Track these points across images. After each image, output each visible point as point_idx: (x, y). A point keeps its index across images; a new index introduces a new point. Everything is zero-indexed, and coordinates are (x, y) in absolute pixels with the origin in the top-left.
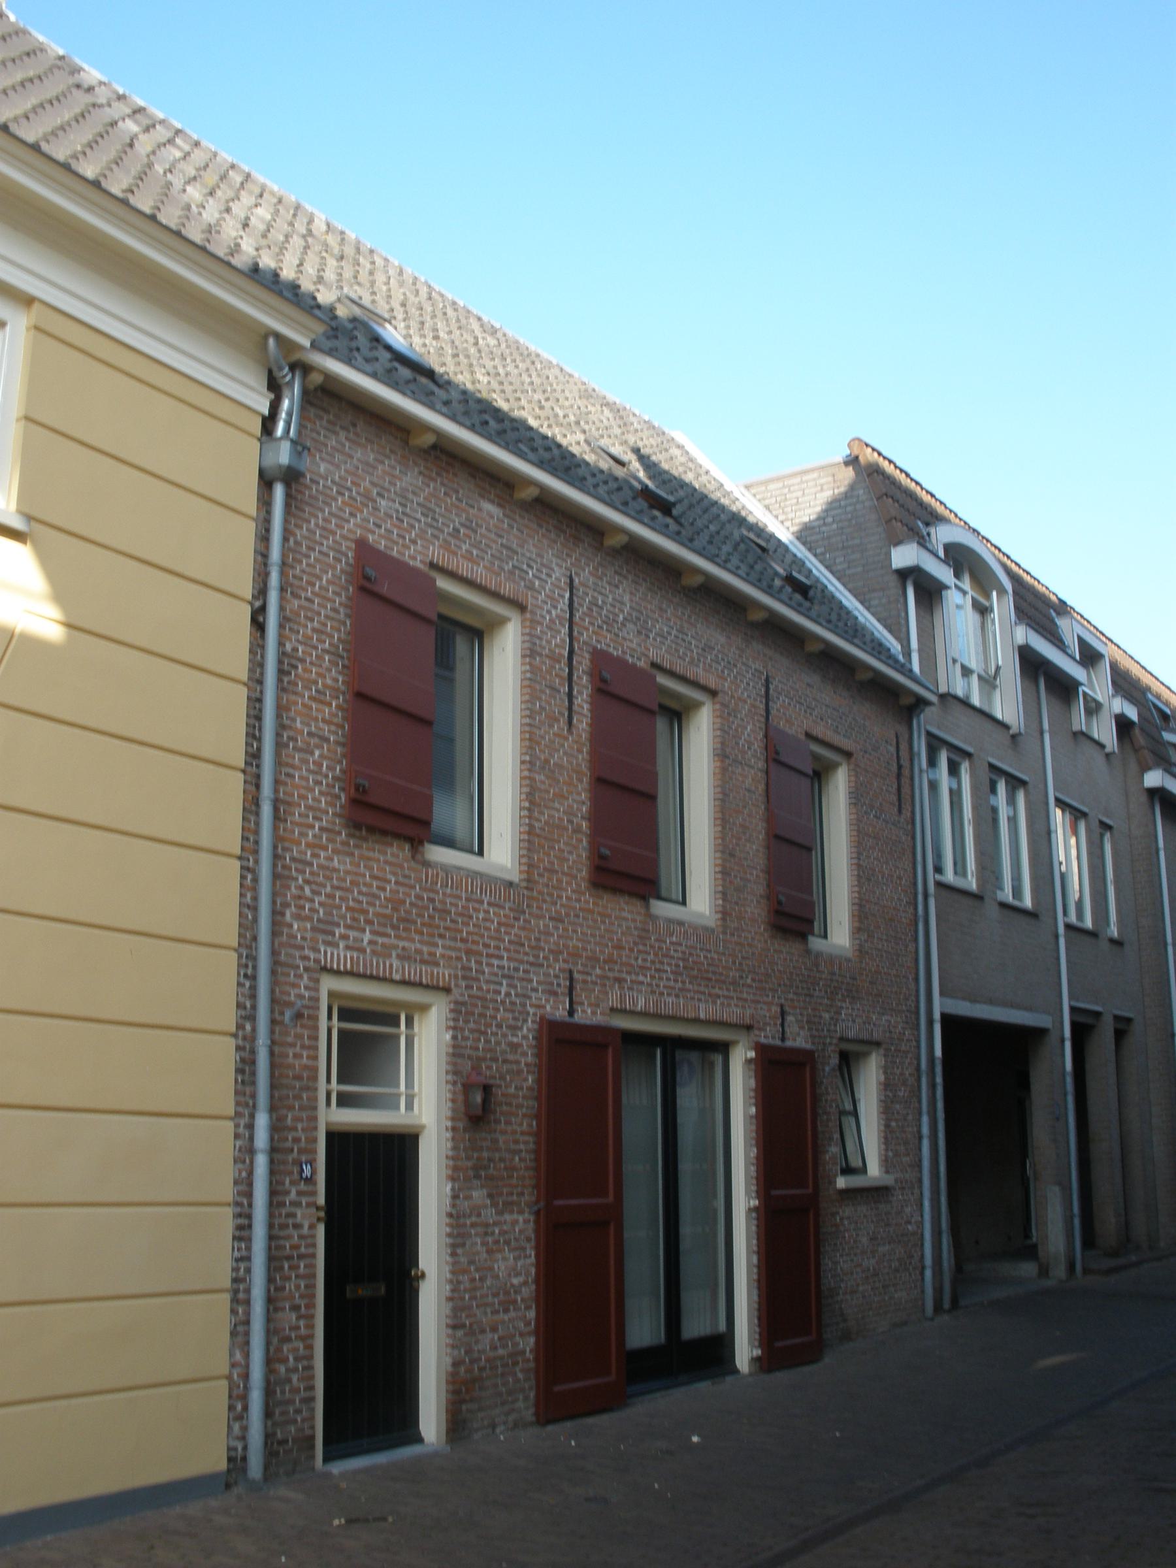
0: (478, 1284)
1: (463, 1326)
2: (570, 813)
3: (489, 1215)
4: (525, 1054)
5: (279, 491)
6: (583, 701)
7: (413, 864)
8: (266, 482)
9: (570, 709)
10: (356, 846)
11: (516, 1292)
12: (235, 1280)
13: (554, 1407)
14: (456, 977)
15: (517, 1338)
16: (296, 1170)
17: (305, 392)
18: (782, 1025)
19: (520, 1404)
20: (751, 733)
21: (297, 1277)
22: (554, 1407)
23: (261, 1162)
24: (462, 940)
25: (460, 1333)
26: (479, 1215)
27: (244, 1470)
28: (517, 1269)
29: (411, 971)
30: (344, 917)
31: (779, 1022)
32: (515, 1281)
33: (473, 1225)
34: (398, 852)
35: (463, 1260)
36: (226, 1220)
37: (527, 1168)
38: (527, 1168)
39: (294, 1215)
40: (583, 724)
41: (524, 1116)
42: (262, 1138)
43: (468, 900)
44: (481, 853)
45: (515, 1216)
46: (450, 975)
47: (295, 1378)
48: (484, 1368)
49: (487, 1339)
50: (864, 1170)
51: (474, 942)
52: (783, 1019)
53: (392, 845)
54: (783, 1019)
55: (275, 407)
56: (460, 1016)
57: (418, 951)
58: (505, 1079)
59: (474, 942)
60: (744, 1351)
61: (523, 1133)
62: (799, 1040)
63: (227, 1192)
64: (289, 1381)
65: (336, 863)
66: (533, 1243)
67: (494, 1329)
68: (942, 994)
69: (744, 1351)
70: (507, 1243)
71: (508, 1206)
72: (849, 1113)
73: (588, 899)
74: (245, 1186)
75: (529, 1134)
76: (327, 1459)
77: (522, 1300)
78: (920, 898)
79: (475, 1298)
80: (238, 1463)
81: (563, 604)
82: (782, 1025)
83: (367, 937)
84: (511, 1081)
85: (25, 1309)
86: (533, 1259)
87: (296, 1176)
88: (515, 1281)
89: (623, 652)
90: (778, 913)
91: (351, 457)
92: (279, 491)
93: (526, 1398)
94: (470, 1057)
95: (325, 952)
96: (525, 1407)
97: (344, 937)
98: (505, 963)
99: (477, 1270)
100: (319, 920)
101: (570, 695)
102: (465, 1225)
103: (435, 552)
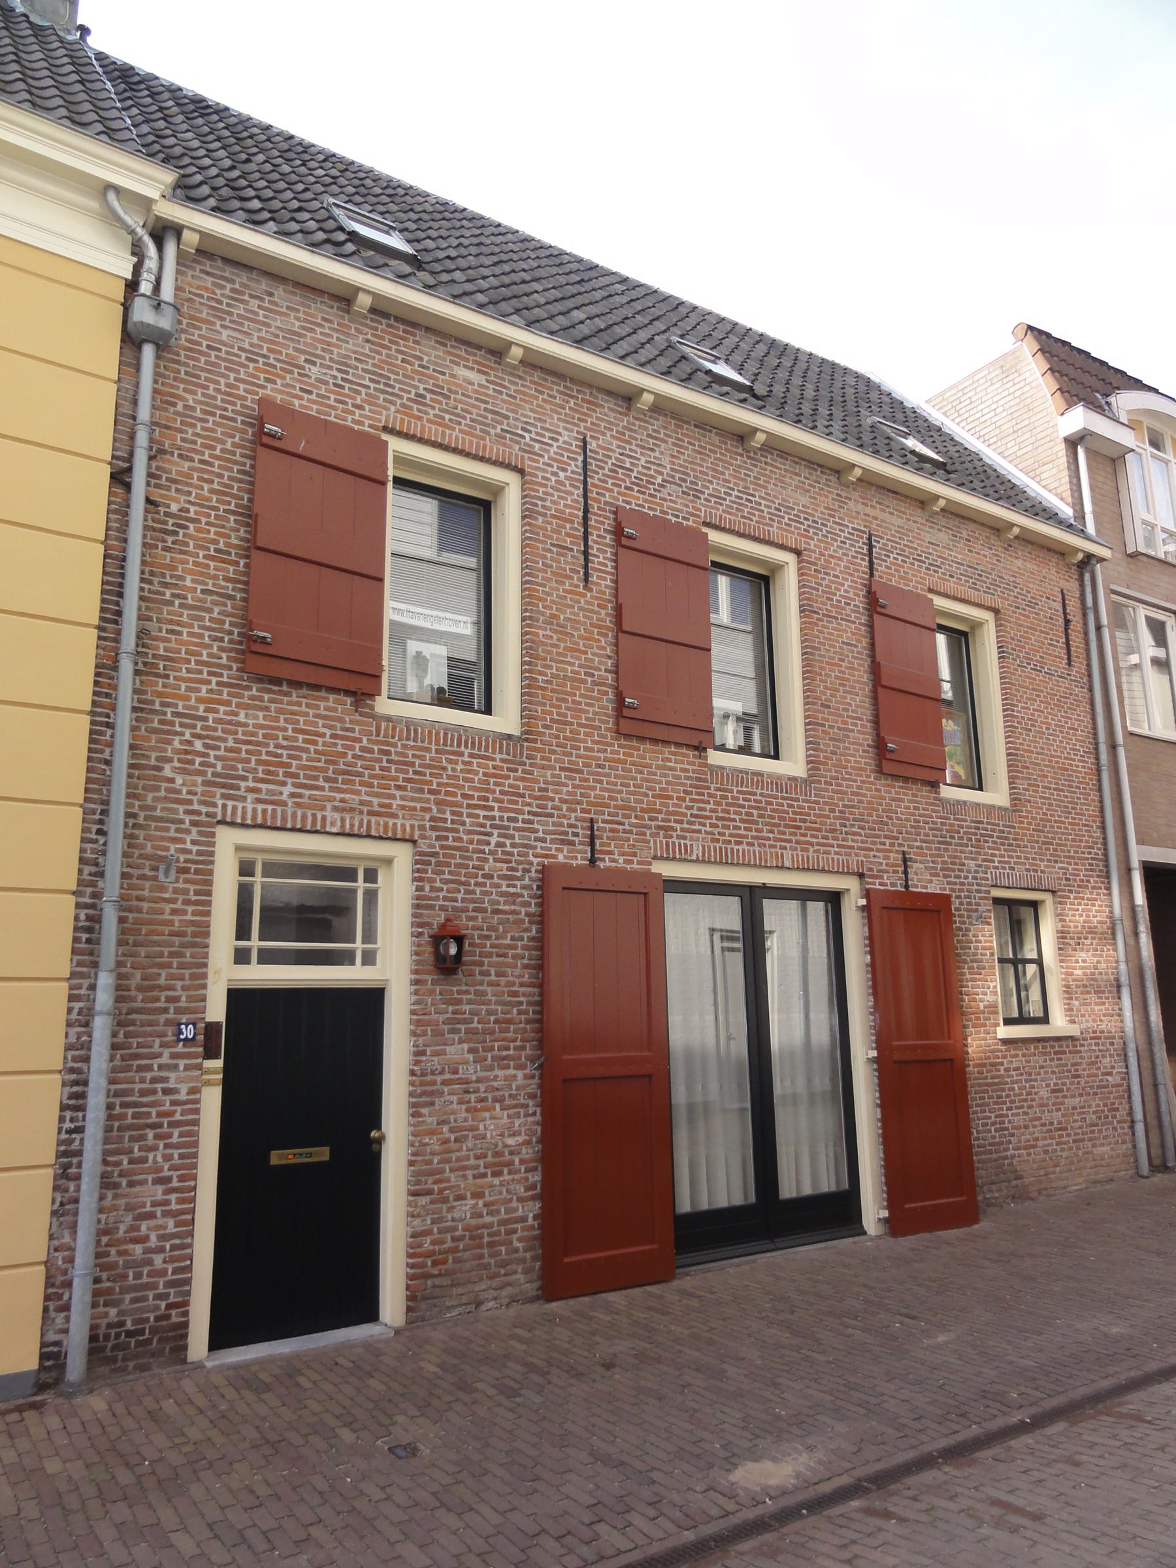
0: (453, 1146)
1: (429, 1192)
2: (589, 668)
3: (471, 1071)
4: (528, 904)
5: (148, 351)
6: (602, 557)
7: (357, 717)
8: (132, 340)
9: (586, 567)
10: (271, 701)
11: (511, 1153)
12: (61, 1155)
13: (556, 1283)
14: (422, 828)
15: (514, 1204)
16: (170, 1030)
17: (181, 257)
18: (906, 873)
19: (520, 1277)
20: (848, 591)
21: (166, 1146)
22: (556, 1283)
23: (101, 1027)
24: (431, 792)
25: (423, 1200)
26: (456, 1072)
27: (62, 1367)
28: (510, 1127)
29: (354, 822)
30: (255, 770)
31: (901, 869)
32: (511, 1141)
33: (445, 1083)
34: (337, 705)
35: (432, 1121)
36: (52, 1091)
37: (528, 1022)
38: (528, 1022)
39: (165, 1080)
40: (603, 583)
41: (525, 967)
42: (104, 998)
43: (437, 751)
44: (488, 711)
45: (512, 1072)
46: (412, 826)
47: (158, 1260)
48: (461, 1238)
49: (464, 1209)
50: (1045, 1020)
51: (447, 793)
52: (906, 867)
53: (326, 699)
54: (906, 867)
55: (137, 269)
56: (421, 863)
57: (362, 803)
58: (496, 930)
59: (447, 793)
60: (872, 1209)
61: (522, 985)
62: (926, 882)
63: (55, 1057)
64: (150, 1262)
65: (242, 718)
66: (539, 1100)
67: (478, 1195)
68: (1140, 842)
69: (872, 1209)
70: (501, 1100)
71: (502, 1062)
72: (1031, 961)
73: (618, 749)
74: (79, 1051)
75: (531, 985)
76: (217, 1342)
77: (522, 1162)
78: (1103, 748)
79: (449, 1161)
80: (52, 1357)
81: (576, 466)
82: (906, 873)
83: (288, 790)
84: (504, 931)
85: (31, 1172)
86: (538, 1117)
87: (170, 1038)
88: (511, 1141)
89: (662, 512)
90: (252, 547)
91: (268, 325)
92: (148, 351)
93: (526, 1272)
94: (442, 908)
95: (224, 806)
96: (524, 1281)
97: (251, 790)
98: (496, 813)
99: (452, 1130)
100: (214, 774)
101: (586, 553)
102: (434, 1083)
103: (390, 415)
